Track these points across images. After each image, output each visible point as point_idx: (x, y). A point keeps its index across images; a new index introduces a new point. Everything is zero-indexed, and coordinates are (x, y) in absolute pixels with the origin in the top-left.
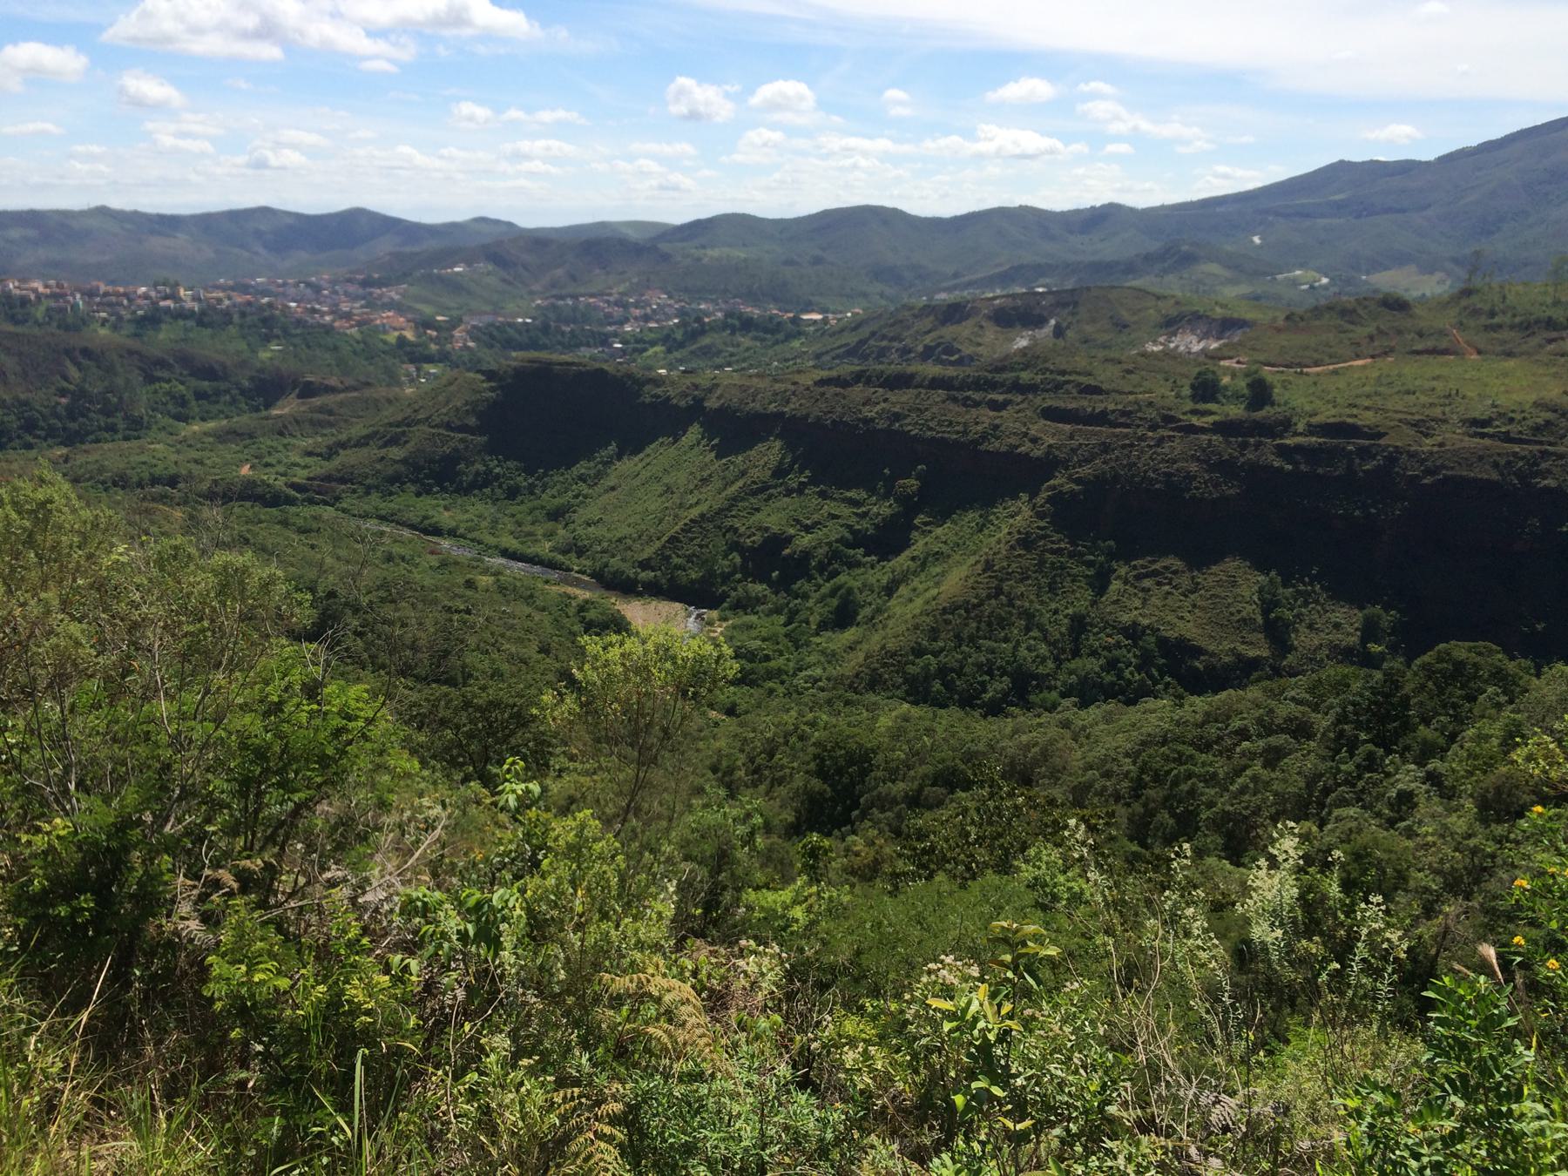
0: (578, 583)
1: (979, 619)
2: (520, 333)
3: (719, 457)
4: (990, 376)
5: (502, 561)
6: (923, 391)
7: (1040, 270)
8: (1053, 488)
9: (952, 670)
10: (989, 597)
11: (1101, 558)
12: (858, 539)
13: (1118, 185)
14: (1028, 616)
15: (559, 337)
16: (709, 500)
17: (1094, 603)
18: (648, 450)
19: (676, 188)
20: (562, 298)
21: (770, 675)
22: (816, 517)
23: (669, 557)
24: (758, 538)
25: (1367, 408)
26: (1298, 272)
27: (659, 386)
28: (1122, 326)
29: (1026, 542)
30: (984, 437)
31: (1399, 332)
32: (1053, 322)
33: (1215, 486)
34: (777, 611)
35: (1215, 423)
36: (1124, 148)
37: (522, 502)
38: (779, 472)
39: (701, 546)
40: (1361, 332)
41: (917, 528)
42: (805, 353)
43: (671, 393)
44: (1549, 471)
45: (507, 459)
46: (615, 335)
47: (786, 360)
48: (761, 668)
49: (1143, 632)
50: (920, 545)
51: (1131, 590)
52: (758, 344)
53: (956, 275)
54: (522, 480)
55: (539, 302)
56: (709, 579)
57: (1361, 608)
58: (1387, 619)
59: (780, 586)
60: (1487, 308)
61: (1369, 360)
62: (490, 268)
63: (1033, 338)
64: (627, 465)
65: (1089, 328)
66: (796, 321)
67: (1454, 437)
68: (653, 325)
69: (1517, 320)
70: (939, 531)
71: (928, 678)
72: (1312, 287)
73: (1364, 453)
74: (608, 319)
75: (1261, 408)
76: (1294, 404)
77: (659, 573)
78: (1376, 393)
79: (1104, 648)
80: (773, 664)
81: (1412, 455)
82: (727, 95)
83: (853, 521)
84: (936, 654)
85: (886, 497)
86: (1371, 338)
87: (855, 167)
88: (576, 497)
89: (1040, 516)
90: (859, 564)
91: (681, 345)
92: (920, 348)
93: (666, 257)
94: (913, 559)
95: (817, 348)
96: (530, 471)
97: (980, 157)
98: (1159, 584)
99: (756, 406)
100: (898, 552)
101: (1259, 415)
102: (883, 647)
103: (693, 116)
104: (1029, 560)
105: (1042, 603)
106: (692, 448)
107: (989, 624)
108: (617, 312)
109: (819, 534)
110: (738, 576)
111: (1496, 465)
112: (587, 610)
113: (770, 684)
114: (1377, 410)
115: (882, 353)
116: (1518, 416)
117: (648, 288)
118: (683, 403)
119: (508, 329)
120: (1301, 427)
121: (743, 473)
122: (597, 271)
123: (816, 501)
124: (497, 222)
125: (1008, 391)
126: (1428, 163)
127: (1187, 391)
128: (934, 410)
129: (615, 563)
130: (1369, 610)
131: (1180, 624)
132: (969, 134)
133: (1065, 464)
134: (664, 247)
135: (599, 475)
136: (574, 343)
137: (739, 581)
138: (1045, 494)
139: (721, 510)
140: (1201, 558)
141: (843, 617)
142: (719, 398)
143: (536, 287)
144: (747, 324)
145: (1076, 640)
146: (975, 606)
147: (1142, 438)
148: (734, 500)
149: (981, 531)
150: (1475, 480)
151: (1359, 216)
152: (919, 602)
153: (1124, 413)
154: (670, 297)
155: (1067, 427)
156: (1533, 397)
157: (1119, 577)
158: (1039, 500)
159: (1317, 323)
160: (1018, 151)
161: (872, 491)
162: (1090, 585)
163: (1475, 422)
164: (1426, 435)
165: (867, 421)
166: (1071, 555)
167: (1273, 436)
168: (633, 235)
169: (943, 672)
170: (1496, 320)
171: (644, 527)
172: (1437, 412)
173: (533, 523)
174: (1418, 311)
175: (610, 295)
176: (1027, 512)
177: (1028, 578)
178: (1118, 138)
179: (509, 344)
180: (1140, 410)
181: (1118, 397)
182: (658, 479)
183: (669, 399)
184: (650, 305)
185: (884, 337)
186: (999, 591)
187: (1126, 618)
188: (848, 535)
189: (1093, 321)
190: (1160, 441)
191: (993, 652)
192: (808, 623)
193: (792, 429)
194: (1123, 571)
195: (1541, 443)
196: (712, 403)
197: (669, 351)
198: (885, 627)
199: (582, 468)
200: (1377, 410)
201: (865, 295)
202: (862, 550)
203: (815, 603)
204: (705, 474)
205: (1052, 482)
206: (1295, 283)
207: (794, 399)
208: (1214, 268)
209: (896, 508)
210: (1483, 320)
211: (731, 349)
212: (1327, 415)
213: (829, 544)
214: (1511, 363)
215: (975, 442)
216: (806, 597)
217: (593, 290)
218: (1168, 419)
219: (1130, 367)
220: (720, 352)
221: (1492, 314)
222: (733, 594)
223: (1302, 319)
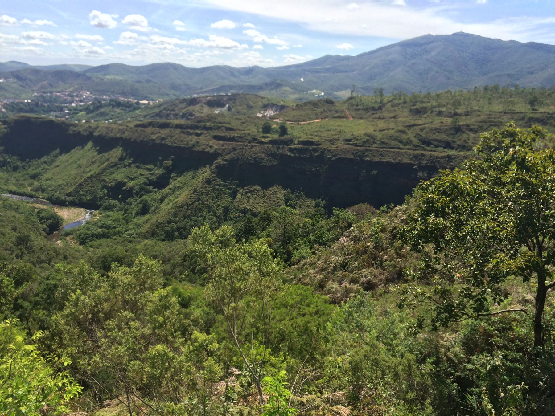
0: (42, 203)
1: (192, 209)
2: (26, 106)
3: (99, 154)
4: (196, 124)
5: (10, 195)
6: (173, 129)
7: (231, 87)
8: (217, 163)
9: (182, 228)
10: (195, 201)
11: (234, 187)
12: (151, 183)
13: (259, 60)
14: (209, 207)
15: (43, 108)
16: (95, 169)
17: (232, 202)
18: (72, 151)
19: (96, 52)
20: (46, 93)
21: (115, 234)
22: (135, 175)
23: (79, 191)
24: (113, 183)
25: (316, 136)
26: (314, 91)
27: (75, 127)
28: (250, 107)
29: (208, 182)
30: (194, 146)
31: (330, 111)
32: (227, 106)
33: (270, 162)
34: (121, 210)
35: (269, 141)
36: (260, 47)
37: (20, 172)
38: (121, 159)
39: (91, 187)
40: (319, 110)
41: (172, 178)
42: (140, 115)
43: (81, 129)
44: (368, 155)
45: (13, 155)
46: (66, 107)
47: (133, 118)
48: (112, 231)
49: (248, 211)
50: (173, 184)
51: (244, 197)
52: (123, 112)
53: (201, 88)
54: (19, 164)
55: (36, 94)
56: (94, 200)
57: (315, 200)
58: (322, 203)
59: (123, 200)
60: (356, 103)
61: (320, 120)
62: (15, 80)
63: (221, 111)
64: (64, 157)
65: (239, 108)
66: (138, 103)
67: (341, 145)
68: (82, 104)
69: (364, 107)
70: (179, 179)
71: (173, 231)
72: (319, 96)
73: (315, 150)
74: (65, 101)
75: (283, 135)
76: (294, 134)
77: (75, 198)
78: (319, 131)
79: (235, 217)
80: (117, 230)
81: (329, 151)
82: (113, 19)
83: (148, 176)
84: (176, 223)
85: (160, 167)
86: (321, 112)
87: (165, 48)
88: (43, 169)
89: (213, 173)
90: (151, 192)
91: (92, 111)
92: (181, 114)
93: (89, 78)
94: (170, 189)
95: (145, 113)
96: (23, 160)
97: (211, 47)
98: (253, 195)
99: (112, 135)
100: (164, 187)
101: (283, 138)
102: (157, 221)
103: (100, 25)
104: (209, 188)
105: (214, 203)
106: (89, 150)
107: (195, 211)
108: (69, 99)
109: (136, 181)
110: (106, 197)
111: (353, 154)
112: (41, 213)
113: (115, 237)
114: (319, 136)
115: (168, 116)
116: (359, 138)
117: (82, 90)
118: (85, 134)
119: (21, 105)
120: (296, 142)
121: (108, 160)
122: (61, 83)
123: (135, 169)
124: (20, 63)
125: (202, 130)
126: (354, 57)
127: (261, 130)
128: (177, 136)
129: (57, 194)
130: (317, 200)
131: (259, 208)
132: (207, 39)
133: (221, 155)
134: (89, 74)
135: (53, 161)
136: (49, 110)
137: (106, 199)
138: (214, 165)
139: (99, 173)
140: (266, 185)
141: (144, 210)
142: (99, 132)
143: (35, 88)
144: (119, 104)
145: (225, 215)
146: (190, 205)
147: (246, 146)
148: (104, 170)
149: (193, 178)
150: (347, 158)
151: (334, 73)
152: (171, 204)
153: (240, 137)
154: (91, 93)
155: (222, 142)
156: (364, 132)
157: (240, 193)
158: (213, 167)
159: (306, 107)
160: (224, 46)
161: (155, 165)
162: (231, 196)
163: (347, 140)
164: (333, 144)
165: (153, 140)
166: (224, 186)
167: (288, 145)
168: (78, 70)
169: (179, 229)
170: (358, 107)
171: (69, 180)
172: (336, 137)
173: (24, 180)
174: (337, 104)
175: (66, 92)
176: (209, 172)
177: (209, 194)
178: (257, 43)
179: (21, 110)
180: (245, 136)
181: (238, 132)
182: (76, 162)
183: (79, 132)
184: (82, 96)
185: (168, 110)
186: (199, 199)
187: (242, 207)
188: (147, 181)
189: (241, 105)
190: (252, 147)
191: (197, 221)
192: (132, 214)
193: (126, 143)
194: (241, 191)
195: (365, 146)
196: (96, 134)
197: (88, 113)
198: (159, 213)
199: (45, 159)
200: (319, 136)
201: (168, 94)
202: (152, 187)
203: (135, 205)
204: (94, 160)
205: (217, 161)
206: (313, 94)
207: (126, 132)
208: (287, 88)
209: (164, 171)
210: (355, 107)
211: (112, 113)
212: (304, 138)
213: (140, 185)
214: (361, 121)
215: (191, 148)
216: (131, 204)
217: (59, 90)
218: (255, 139)
219: (244, 121)
220: (108, 114)
221: (357, 105)
222: (104, 204)
223: (301, 106)
